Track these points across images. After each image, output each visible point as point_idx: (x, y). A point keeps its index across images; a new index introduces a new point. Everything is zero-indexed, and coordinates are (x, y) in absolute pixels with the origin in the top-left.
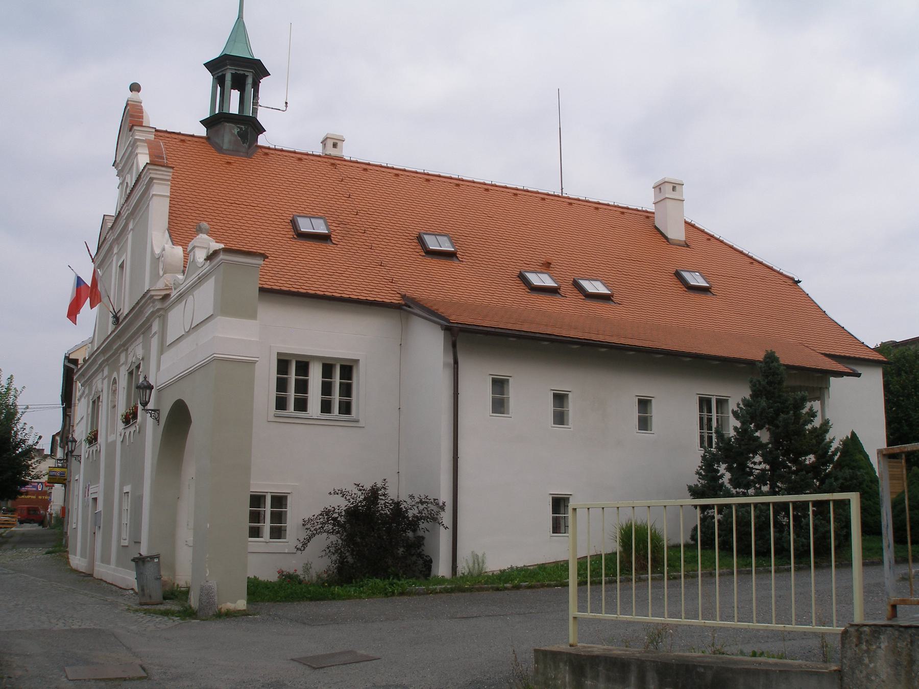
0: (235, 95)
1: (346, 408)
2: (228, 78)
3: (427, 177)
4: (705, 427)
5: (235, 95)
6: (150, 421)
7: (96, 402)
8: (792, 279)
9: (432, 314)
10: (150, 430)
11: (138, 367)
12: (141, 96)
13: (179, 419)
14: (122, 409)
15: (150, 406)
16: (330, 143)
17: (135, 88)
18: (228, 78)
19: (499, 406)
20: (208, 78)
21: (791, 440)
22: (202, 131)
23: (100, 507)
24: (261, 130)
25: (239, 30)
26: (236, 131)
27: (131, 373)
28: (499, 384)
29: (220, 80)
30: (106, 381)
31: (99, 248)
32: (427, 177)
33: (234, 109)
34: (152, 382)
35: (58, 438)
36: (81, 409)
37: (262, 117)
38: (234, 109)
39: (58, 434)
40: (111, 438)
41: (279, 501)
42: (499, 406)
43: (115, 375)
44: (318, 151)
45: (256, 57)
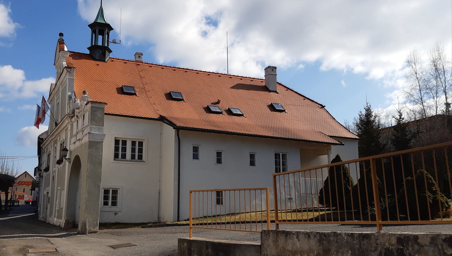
0: (100, 37)
1: (140, 157)
2: (97, 31)
3: (175, 69)
4: (278, 162)
5: (100, 37)
6: (67, 163)
7: (49, 155)
8: (321, 105)
9: (171, 124)
10: (67, 166)
11: (64, 142)
12: (64, 38)
13: (77, 164)
14: (58, 158)
15: (67, 157)
16: (137, 56)
17: (61, 35)
18: (97, 31)
19: (196, 157)
20: (90, 30)
21: (14, 201)
22: (88, 52)
23: (50, 196)
24: (110, 51)
25: (101, 13)
26: (101, 52)
27: (61, 145)
28: (196, 149)
29: (94, 32)
30: (52, 148)
31: (50, 96)
32: (175, 69)
33: (100, 43)
34: (68, 149)
35: (37, 169)
36: (45, 158)
37: (111, 46)
38: (100, 43)
39: (37, 167)
40: (54, 169)
41: (115, 192)
42: (196, 157)
43: (56, 145)
44: (133, 59)
45: (108, 22)
